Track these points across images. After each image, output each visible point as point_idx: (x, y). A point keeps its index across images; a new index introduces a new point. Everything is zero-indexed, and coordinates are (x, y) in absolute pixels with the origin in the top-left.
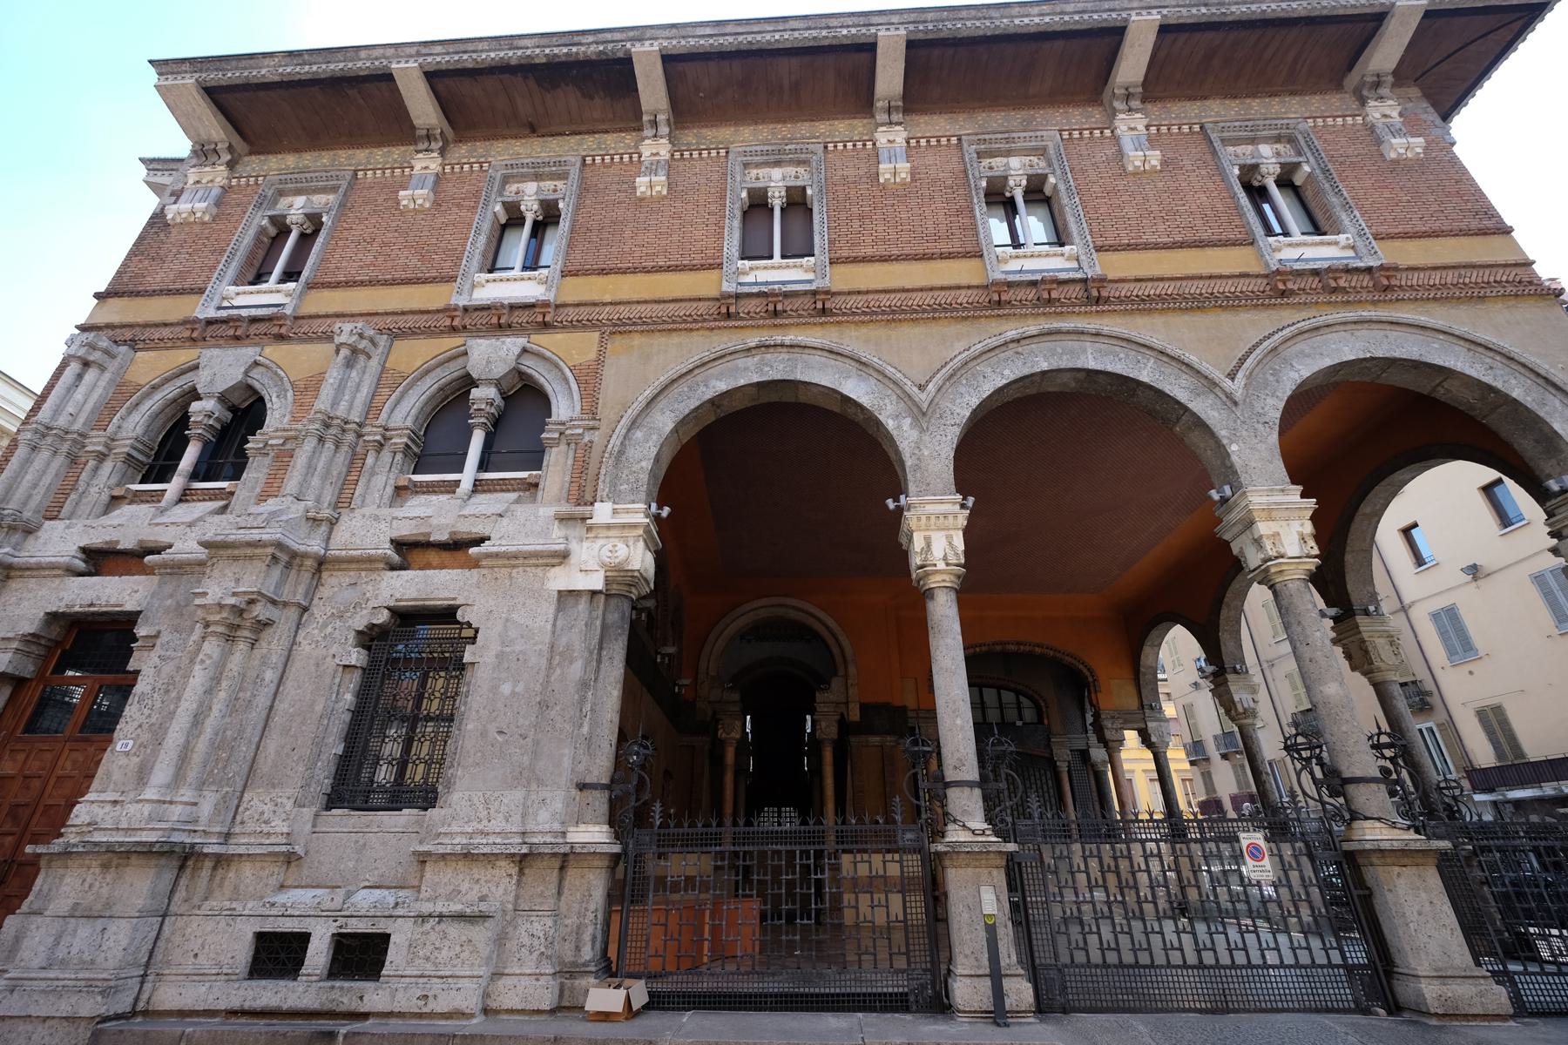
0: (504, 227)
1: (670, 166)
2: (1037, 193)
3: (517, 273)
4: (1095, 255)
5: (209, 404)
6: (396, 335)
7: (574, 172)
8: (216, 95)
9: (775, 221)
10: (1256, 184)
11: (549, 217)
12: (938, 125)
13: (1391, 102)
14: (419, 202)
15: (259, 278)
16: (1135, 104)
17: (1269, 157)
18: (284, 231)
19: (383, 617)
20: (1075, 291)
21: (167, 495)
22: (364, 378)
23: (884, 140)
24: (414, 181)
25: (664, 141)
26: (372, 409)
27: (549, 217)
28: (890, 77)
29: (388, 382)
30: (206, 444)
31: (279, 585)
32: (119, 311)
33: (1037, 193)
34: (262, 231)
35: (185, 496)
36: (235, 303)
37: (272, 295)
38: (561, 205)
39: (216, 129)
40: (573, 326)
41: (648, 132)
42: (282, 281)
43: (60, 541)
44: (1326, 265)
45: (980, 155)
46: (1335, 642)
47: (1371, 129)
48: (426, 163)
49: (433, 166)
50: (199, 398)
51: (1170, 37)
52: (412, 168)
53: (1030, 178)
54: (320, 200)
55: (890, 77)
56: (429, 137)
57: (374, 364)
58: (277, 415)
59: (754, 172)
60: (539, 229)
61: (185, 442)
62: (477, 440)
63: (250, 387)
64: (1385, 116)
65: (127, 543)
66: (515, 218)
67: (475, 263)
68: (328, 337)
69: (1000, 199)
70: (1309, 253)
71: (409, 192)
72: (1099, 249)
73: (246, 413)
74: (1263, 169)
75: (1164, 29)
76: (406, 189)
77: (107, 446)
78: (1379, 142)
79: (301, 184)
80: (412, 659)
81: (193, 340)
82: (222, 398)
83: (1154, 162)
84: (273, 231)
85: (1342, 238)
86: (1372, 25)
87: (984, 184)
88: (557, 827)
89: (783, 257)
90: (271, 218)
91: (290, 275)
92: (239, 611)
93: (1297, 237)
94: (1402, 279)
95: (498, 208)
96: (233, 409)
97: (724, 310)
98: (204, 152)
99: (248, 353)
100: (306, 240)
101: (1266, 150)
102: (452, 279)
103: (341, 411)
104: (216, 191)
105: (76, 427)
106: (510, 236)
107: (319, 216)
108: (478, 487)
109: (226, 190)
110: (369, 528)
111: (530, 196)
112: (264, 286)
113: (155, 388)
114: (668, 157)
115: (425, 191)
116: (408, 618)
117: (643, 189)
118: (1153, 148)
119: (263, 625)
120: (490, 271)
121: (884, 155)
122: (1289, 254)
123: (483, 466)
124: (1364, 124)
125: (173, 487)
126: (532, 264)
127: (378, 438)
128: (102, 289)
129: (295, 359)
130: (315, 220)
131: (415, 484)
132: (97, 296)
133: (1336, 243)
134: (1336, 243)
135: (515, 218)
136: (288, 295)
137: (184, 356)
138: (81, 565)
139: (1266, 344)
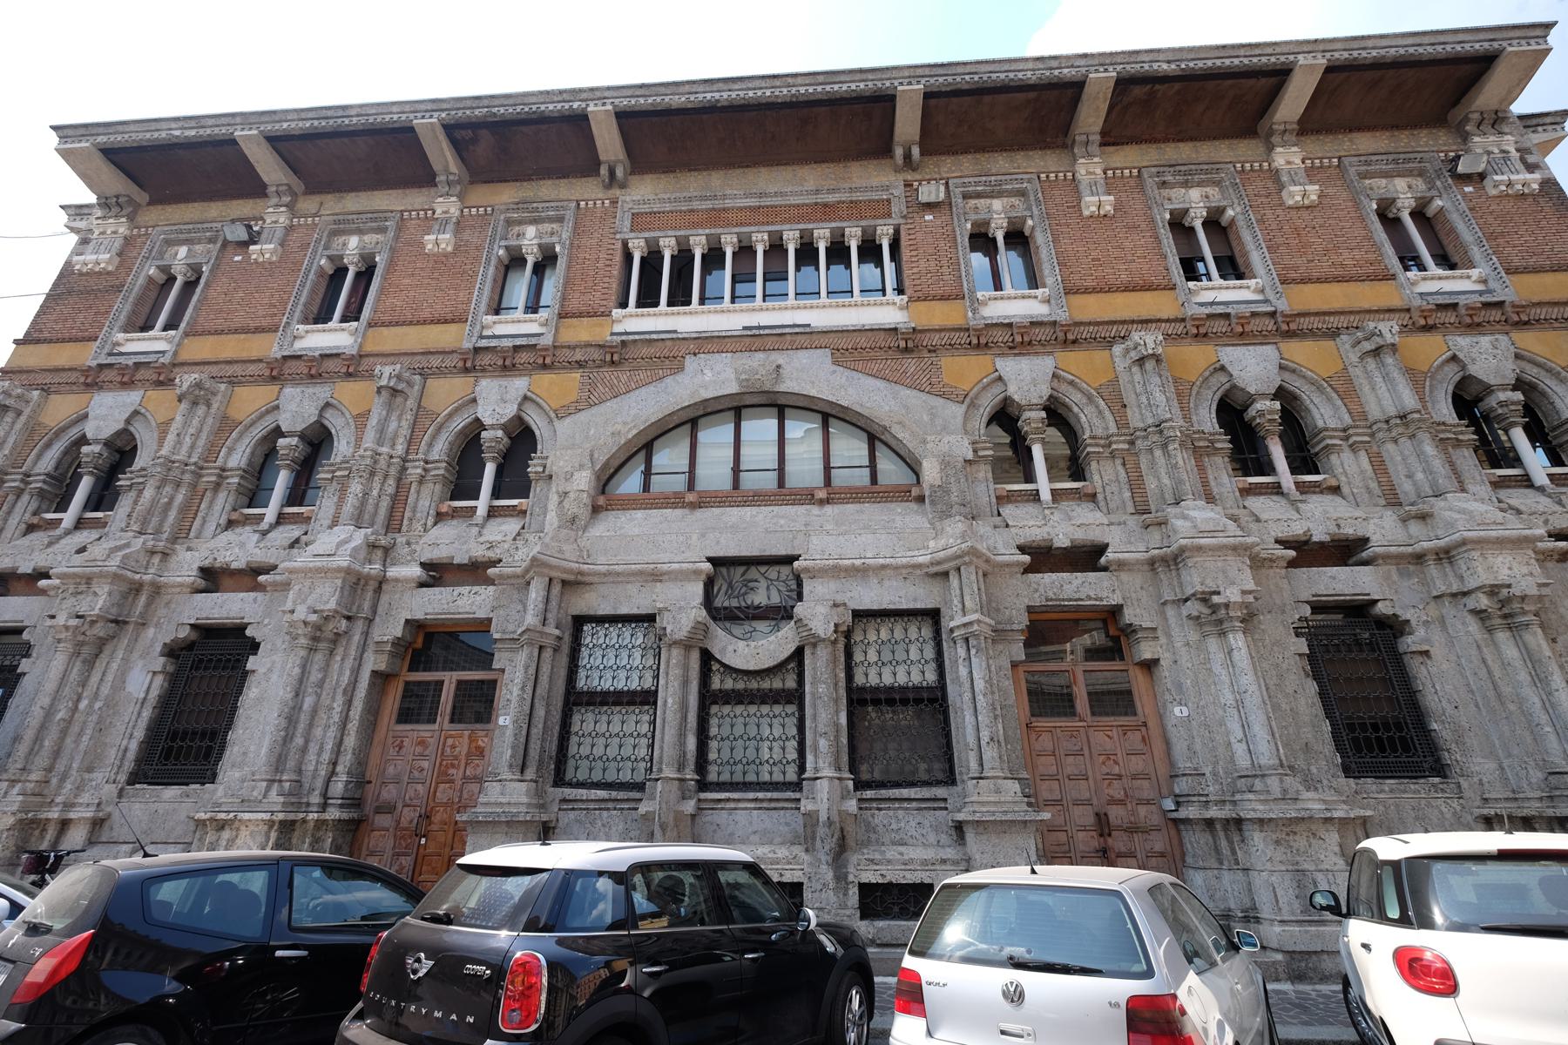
0: (507, 268)
1: (459, 226)
2: (1018, 238)
3: (519, 314)
5: (97, 448)
6: (233, 382)
7: (569, 215)
8: (112, 154)
9: (341, 290)
10: (1391, 215)
11: (547, 261)
12: (1129, 157)
13: (1295, 149)
15: (147, 327)
16: (1094, 148)
17: (1405, 193)
18: (342, 271)
19: (184, 633)
21: (64, 525)
22: (204, 420)
23: (1083, 172)
24: (264, 236)
26: (212, 452)
27: (547, 261)
28: (907, 124)
29: (226, 426)
30: (98, 479)
32: (39, 356)
33: (1018, 238)
35: (80, 524)
36: (123, 349)
37: (156, 343)
38: (558, 249)
39: (118, 184)
40: (1312, 334)
42: (165, 329)
43: (186, 565)
45: (966, 196)
46: (254, 647)
47: (1275, 174)
48: (447, 206)
50: (283, 435)
51: (933, 102)
53: (1011, 221)
54: (370, 239)
55: (907, 124)
57: (411, 403)
58: (342, 447)
59: (973, 202)
60: (539, 270)
61: (76, 478)
62: (490, 470)
63: (323, 426)
64: (1289, 163)
65: (25, 568)
66: (515, 261)
67: (483, 307)
69: (982, 241)
70: (1449, 286)
73: (122, 451)
74: (1399, 204)
75: (928, 96)
76: (255, 243)
77: (220, 476)
78: (1281, 187)
79: (182, 239)
80: (210, 666)
81: (312, 376)
82: (302, 436)
83: (1108, 208)
84: (161, 278)
86: (1273, 80)
87: (1168, 216)
88: (880, 818)
89: (670, 304)
90: (507, 248)
91: (352, 315)
92: (318, 628)
93: (1008, 290)
94: (926, 340)
95: (501, 252)
96: (310, 444)
97: (608, 358)
98: (105, 203)
100: (190, 286)
101: (1400, 184)
102: (274, 329)
104: (118, 244)
105: (193, 460)
106: (512, 276)
107: (373, 256)
108: (492, 513)
109: (128, 241)
111: (530, 239)
112: (151, 333)
113: (253, 423)
114: (457, 213)
115: (448, 236)
116: (208, 632)
117: (430, 246)
118: (1311, 183)
119: (337, 637)
120: (497, 313)
121: (1083, 187)
122: (1208, 296)
123: (497, 493)
124: (1270, 170)
125: (68, 517)
126: (533, 307)
128: (21, 337)
130: (196, 270)
131: (455, 509)
132: (16, 342)
133: (1469, 277)
135: (515, 261)
136: (545, 324)
138: (201, 583)
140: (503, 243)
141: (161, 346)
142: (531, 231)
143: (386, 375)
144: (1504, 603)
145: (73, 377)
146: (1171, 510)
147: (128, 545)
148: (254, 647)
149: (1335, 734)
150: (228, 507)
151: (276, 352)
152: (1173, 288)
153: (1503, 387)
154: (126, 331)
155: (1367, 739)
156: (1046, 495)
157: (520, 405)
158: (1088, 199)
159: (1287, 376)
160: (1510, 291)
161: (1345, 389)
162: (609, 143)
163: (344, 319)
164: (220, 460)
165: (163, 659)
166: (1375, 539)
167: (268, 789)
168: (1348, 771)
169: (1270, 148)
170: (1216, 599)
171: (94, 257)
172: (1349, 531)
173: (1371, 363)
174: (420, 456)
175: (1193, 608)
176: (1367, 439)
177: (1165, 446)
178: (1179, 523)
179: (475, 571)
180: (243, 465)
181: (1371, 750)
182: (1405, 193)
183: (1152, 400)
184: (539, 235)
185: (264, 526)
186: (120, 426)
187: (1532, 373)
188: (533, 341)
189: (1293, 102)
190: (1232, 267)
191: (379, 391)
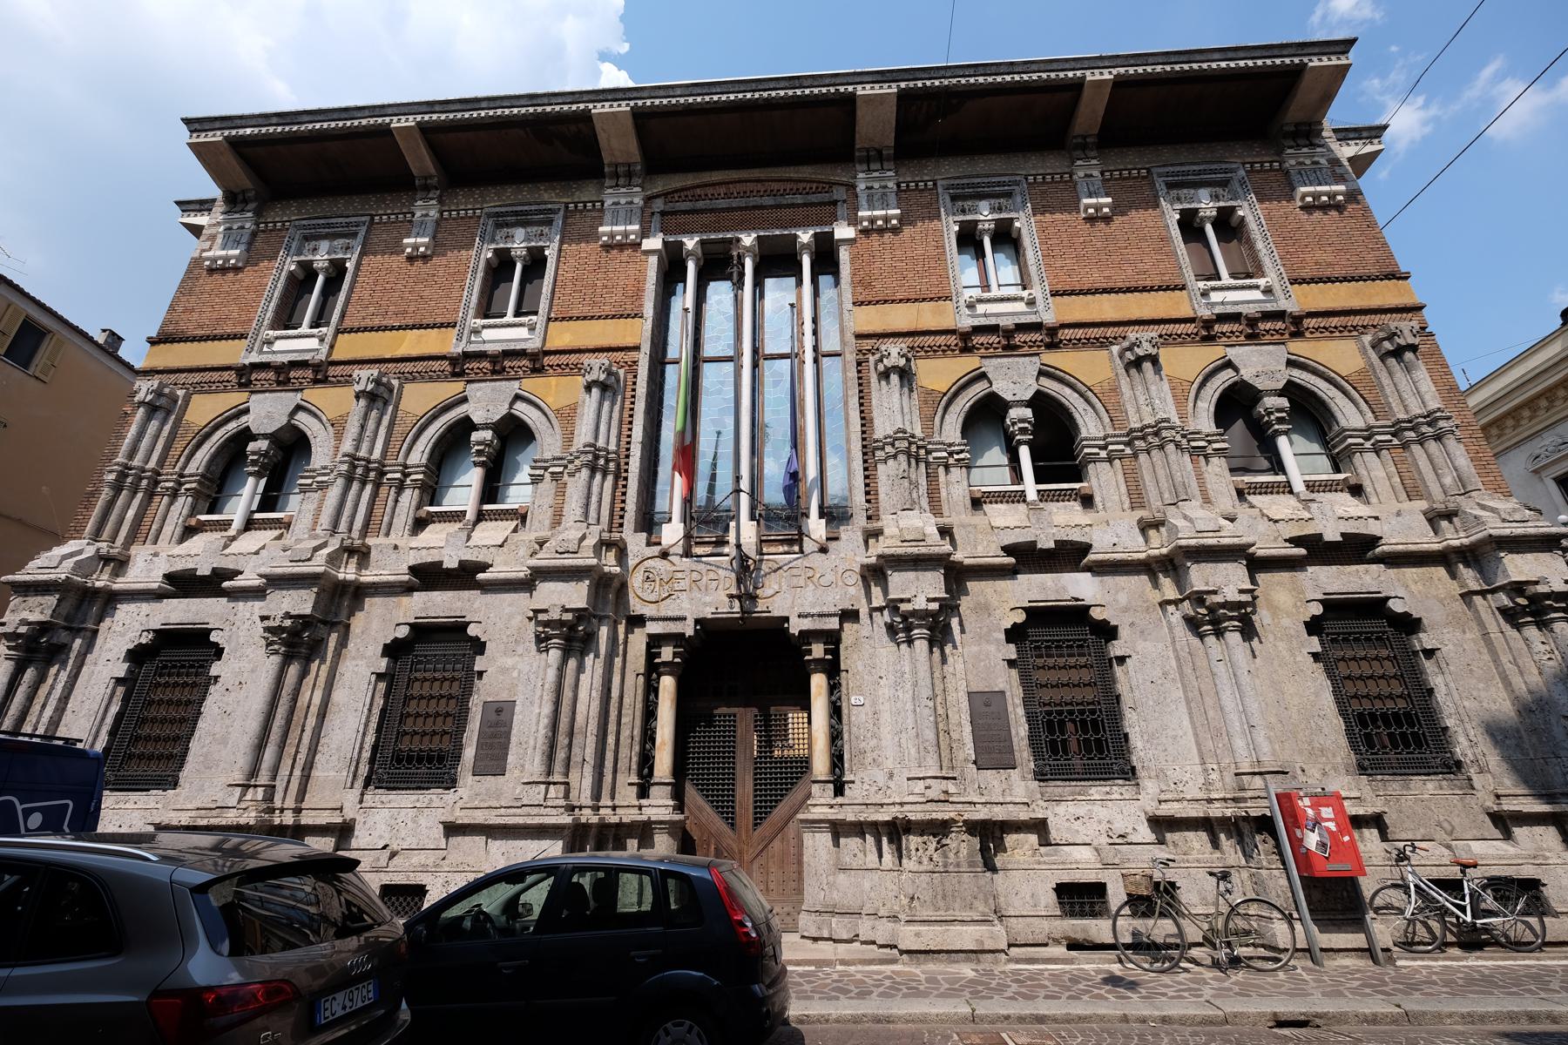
4: (1050, 300)
5: (263, 445)
13: (1094, 162)
14: (422, 249)
20: (231, 376)
23: (1081, 174)
25: (250, 214)
31: (885, 592)
34: (291, 274)
37: (302, 343)
39: (244, 181)
40: (1077, 344)
41: (608, 182)
44: (499, 347)
46: (218, 652)
49: (432, 213)
50: (254, 438)
52: (603, 203)
56: (427, 188)
63: (296, 428)
68: (577, 369)
71: (412, 240)
72: (1293, 282)
80: (433, 660)
84: (301, 276)
85: (1262, 282)
99: (290, 399)
103: (362, 453)
110: (146, 569)
127: (398, 475)
129: (554, 390)
133: (1257, 287)
134: (1257, 287)
137: (452, 388)
139: (1068, 391)
140: (296, 258)
141: (313, 343)
142: (520, 233)
143: (144, 390)
144: (1212, 610)
145: (1190, 328)
146: (1171, 510)
147: (80, 552)
148: (218, 652)
149: (1349, 732)
150: (185, 512)
151: (456, 348)
152: (1183, 288)
153: (1020, 403)
154: (273, 328)
155: (1403, 735)
156: (1032, 495)
157: (512, 404)
158: (1086, 201)
159: (1044, 381)
160: (1294, 301)
161: (1107, 401)
162: (420, 161)
163: (315, 324)
164: (400, 460)
165: (386, 660)
166: (1096, 546)
167: (243, 794)
168: (1362, 769)
169: (1280, 152)
170: (904, 607)
171: (223, 253)
172: (1076, 536)
173: (1392, 361)
174: (400, 460)
175: (1504, 600)
176: (1388, 437)
177: (1161, 447)
178: (1180, 523)
179: (466, 576)
180: (424, 461)
181: (1407, 746)
182: (1206, 205)
183: (1152, 400)
184: (527, 239)
185: (232, 532)
186: (284, 420)
187: (1051, 386)
188: (307, 357)
189: (876, 127)
190: (1248, 270)
191: (588, 388)
